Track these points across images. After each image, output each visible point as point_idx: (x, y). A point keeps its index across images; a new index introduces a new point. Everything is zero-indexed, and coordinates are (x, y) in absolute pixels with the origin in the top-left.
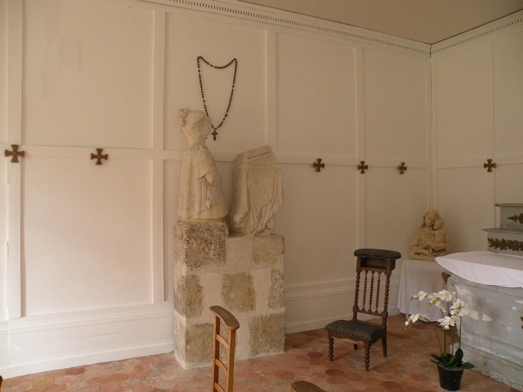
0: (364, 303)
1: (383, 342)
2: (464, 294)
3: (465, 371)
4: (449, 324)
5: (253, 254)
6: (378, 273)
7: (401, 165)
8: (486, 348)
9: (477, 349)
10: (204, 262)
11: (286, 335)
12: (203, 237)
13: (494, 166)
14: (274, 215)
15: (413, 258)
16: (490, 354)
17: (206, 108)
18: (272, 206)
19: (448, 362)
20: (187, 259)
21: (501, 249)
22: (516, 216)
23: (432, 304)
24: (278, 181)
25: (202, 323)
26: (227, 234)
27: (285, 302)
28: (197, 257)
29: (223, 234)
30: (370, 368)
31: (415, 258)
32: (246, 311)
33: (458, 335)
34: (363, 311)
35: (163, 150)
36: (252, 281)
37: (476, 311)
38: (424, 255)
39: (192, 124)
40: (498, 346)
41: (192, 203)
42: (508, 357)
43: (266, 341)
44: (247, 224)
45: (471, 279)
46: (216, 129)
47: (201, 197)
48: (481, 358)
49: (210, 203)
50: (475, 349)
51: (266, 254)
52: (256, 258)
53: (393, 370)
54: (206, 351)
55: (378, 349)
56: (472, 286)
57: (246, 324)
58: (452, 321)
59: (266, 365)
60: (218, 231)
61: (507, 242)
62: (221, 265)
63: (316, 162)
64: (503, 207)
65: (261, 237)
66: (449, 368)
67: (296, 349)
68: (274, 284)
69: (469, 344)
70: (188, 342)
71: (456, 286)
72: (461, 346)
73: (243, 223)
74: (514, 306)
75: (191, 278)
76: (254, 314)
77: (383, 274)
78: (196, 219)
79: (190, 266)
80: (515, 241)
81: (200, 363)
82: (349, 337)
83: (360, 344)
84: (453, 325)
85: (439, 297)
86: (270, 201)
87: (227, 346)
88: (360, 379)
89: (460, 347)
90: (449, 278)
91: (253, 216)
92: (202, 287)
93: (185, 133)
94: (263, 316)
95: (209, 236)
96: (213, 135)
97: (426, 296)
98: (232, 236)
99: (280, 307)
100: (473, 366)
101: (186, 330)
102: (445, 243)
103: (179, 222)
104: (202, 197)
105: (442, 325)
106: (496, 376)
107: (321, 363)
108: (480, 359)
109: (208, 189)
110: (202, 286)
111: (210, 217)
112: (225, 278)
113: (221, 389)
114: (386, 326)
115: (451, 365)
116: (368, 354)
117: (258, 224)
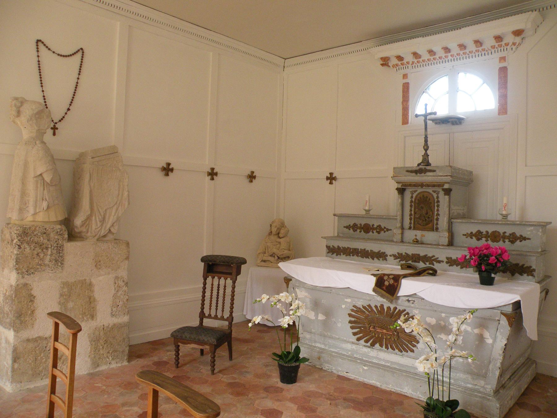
0: (210, 309)
3: (302, 365)
4: (287, 323)
5: (94, 260)
6: (224, 279)
7: (250, 174)
9: (313, 345)
10: (38, 269)
11: (130, 346)
12: (37, 241)
14: (118, 219)
17: (45, 99)
18: (117, 210)
19: (287, 358)
20: (17, 266)
21: (337, 255)
22: (350, 225)
23: (273, 306)
24: (124, 184)
25: (34, 337)
26: (66, 238)
27: (128, 311)
28: (30, 263)
29: (61, 239)
30: (215, 371)
31: (261, 265)
32: (86, 321)
33: (296, 329)
34: (210, 316)
36: (93, 289)
37: (313, 311)
38: (270, 262)
40: (330, 341)
43: (108, 353)
44: (89, 227)
46: (56, 123)
47: (36, 197)
48: (316, 354)
50: (311, 346)
51: (108, 259)
52: (98, 265)
53: (238, 371)
54: (38, 368)
55: (224, 354)
56: (310, 289)
57: (86, 335)
58: (290, 320)
59: (107, 378)
60: (55, 234)
61: (342, 248)
62: (58, 272)
63: (165, 166)
64: (341, 216)
65: (103, 242)
66: (288, 364)
67: (140, 359)
68: (117, 291)
69: (307, 342)
70: (15, 359)
71: (297, 289)
73: (85, 227)
75: (21, 287)
76: (95, 324)
77: (229, 279)
79: (21, 273)
80: (348, 248)
81: (30, 383)
82: (195, 343)
83: (206, 348)
84: (291, 323)
86: (115, 205)
87: (68, 353)
88: (206, 382)
90: (291, 282)
91: (96, 219)
92: (35, 297)
94: (105, 326)
95: (44, 240)
96: (53, 130)
97: (269, 299)
98: (71, 240)
99: (123, 316)
101: (13, 346)
103: (8, 224)
106: (327, 367)
107: (166, 370)
108: (316, 355)
109: (46, 188)
110: (35, 295)
111: (47, 220)
112: (62, 286)
113: (59, 400)
114: (231, 331)
115: (289, 361)
116: (213, 358)
117: (100, 228)
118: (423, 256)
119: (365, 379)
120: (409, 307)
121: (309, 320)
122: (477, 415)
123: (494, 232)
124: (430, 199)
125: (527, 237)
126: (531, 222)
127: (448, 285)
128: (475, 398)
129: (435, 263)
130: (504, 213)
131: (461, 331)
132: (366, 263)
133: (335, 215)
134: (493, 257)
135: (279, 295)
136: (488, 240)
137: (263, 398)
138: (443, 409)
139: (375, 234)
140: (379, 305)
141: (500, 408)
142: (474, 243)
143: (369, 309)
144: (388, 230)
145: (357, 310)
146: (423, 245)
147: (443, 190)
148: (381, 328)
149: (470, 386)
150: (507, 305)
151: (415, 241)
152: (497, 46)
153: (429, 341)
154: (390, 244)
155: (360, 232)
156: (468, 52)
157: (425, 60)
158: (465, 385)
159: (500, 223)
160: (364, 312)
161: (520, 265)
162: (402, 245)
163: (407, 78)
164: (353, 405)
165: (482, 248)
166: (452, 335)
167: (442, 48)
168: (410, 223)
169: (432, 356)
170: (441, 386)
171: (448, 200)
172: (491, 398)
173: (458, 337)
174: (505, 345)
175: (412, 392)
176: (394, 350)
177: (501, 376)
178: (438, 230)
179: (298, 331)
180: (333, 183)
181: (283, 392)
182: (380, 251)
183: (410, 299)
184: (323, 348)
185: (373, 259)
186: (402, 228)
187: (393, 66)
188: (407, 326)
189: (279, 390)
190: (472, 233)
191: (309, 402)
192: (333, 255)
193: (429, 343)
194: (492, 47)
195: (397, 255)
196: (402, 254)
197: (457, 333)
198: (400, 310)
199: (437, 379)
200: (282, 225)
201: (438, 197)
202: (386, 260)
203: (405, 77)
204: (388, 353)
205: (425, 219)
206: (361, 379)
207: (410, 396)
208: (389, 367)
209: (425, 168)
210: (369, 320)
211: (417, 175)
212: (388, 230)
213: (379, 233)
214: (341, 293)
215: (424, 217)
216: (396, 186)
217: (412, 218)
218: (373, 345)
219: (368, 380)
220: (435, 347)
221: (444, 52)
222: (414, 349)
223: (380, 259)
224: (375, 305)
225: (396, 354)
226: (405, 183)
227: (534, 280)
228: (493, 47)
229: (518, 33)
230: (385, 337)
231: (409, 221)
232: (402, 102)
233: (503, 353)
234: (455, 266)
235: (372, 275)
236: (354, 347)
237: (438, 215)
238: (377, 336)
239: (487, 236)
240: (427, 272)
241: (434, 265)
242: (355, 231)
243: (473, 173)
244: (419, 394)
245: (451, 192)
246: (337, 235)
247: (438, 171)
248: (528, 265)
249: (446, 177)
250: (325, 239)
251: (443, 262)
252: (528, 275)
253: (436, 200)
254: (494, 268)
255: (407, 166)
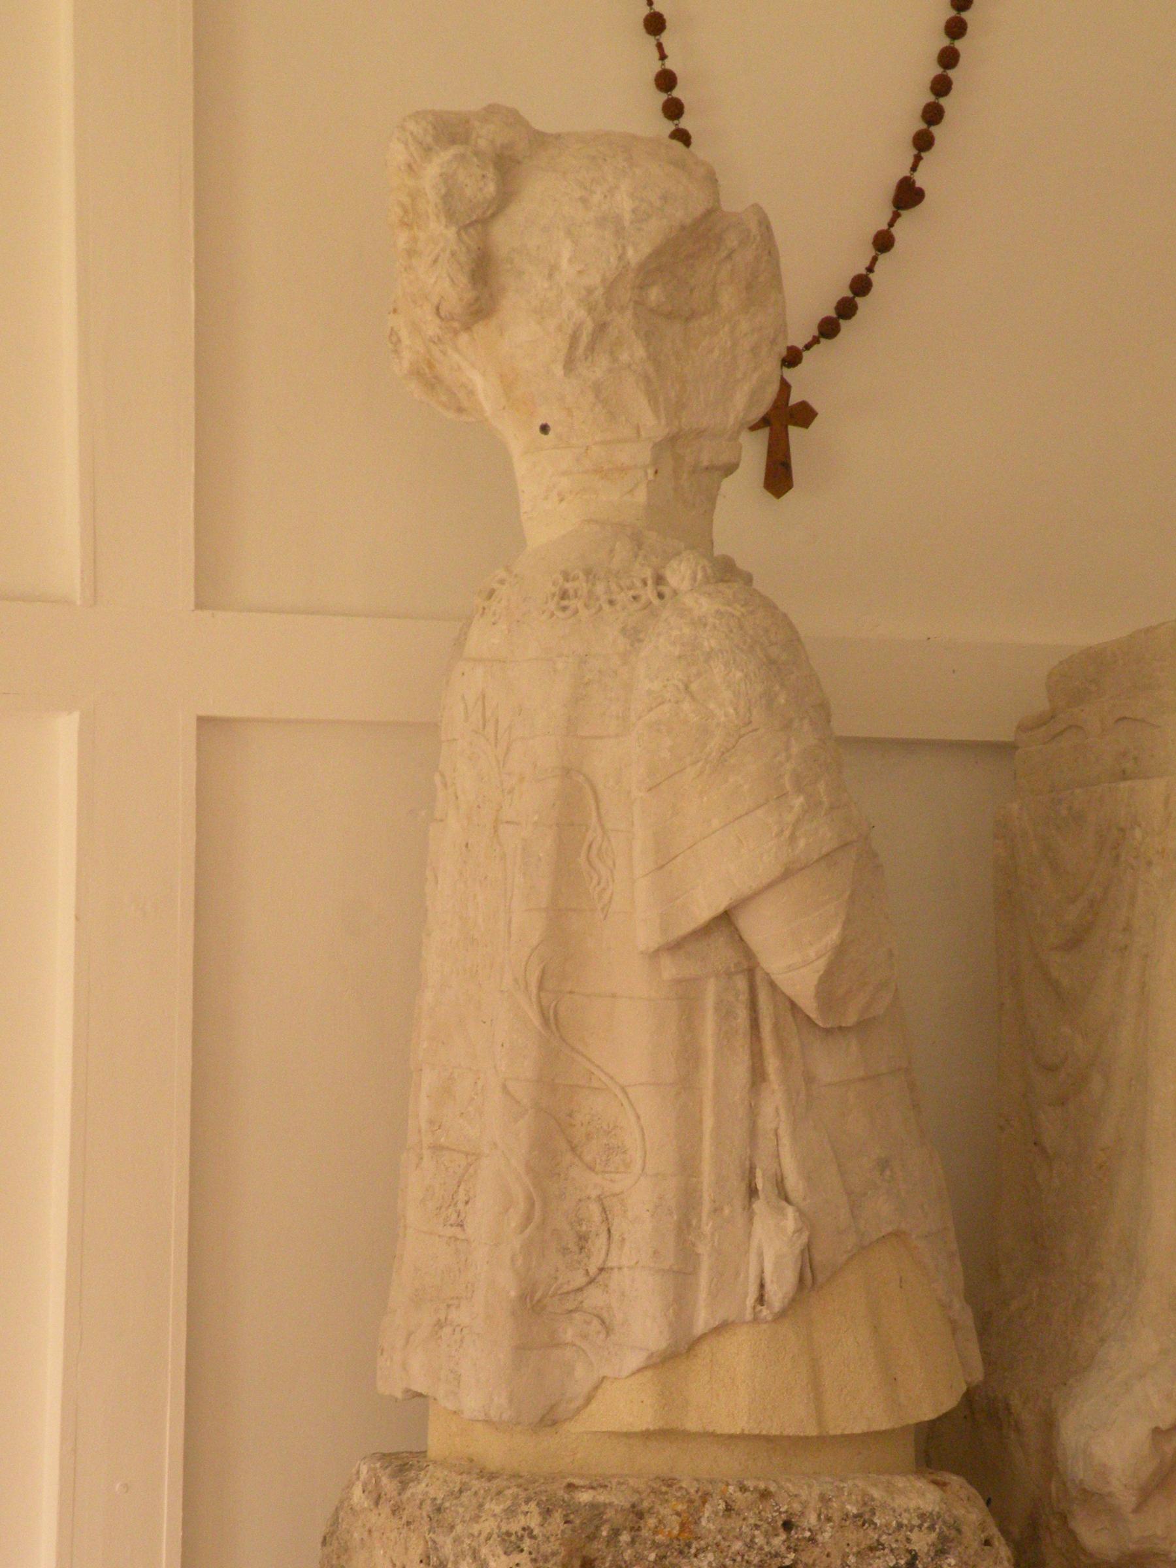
35: (199, 605)
39: (570, 302)
41: (583, 1239)
47: (688, 1166)
49: (804, 1238)
78: (629, 1435)
93: (487, 407)
104: (706, 1167)
109: (772, 1065)
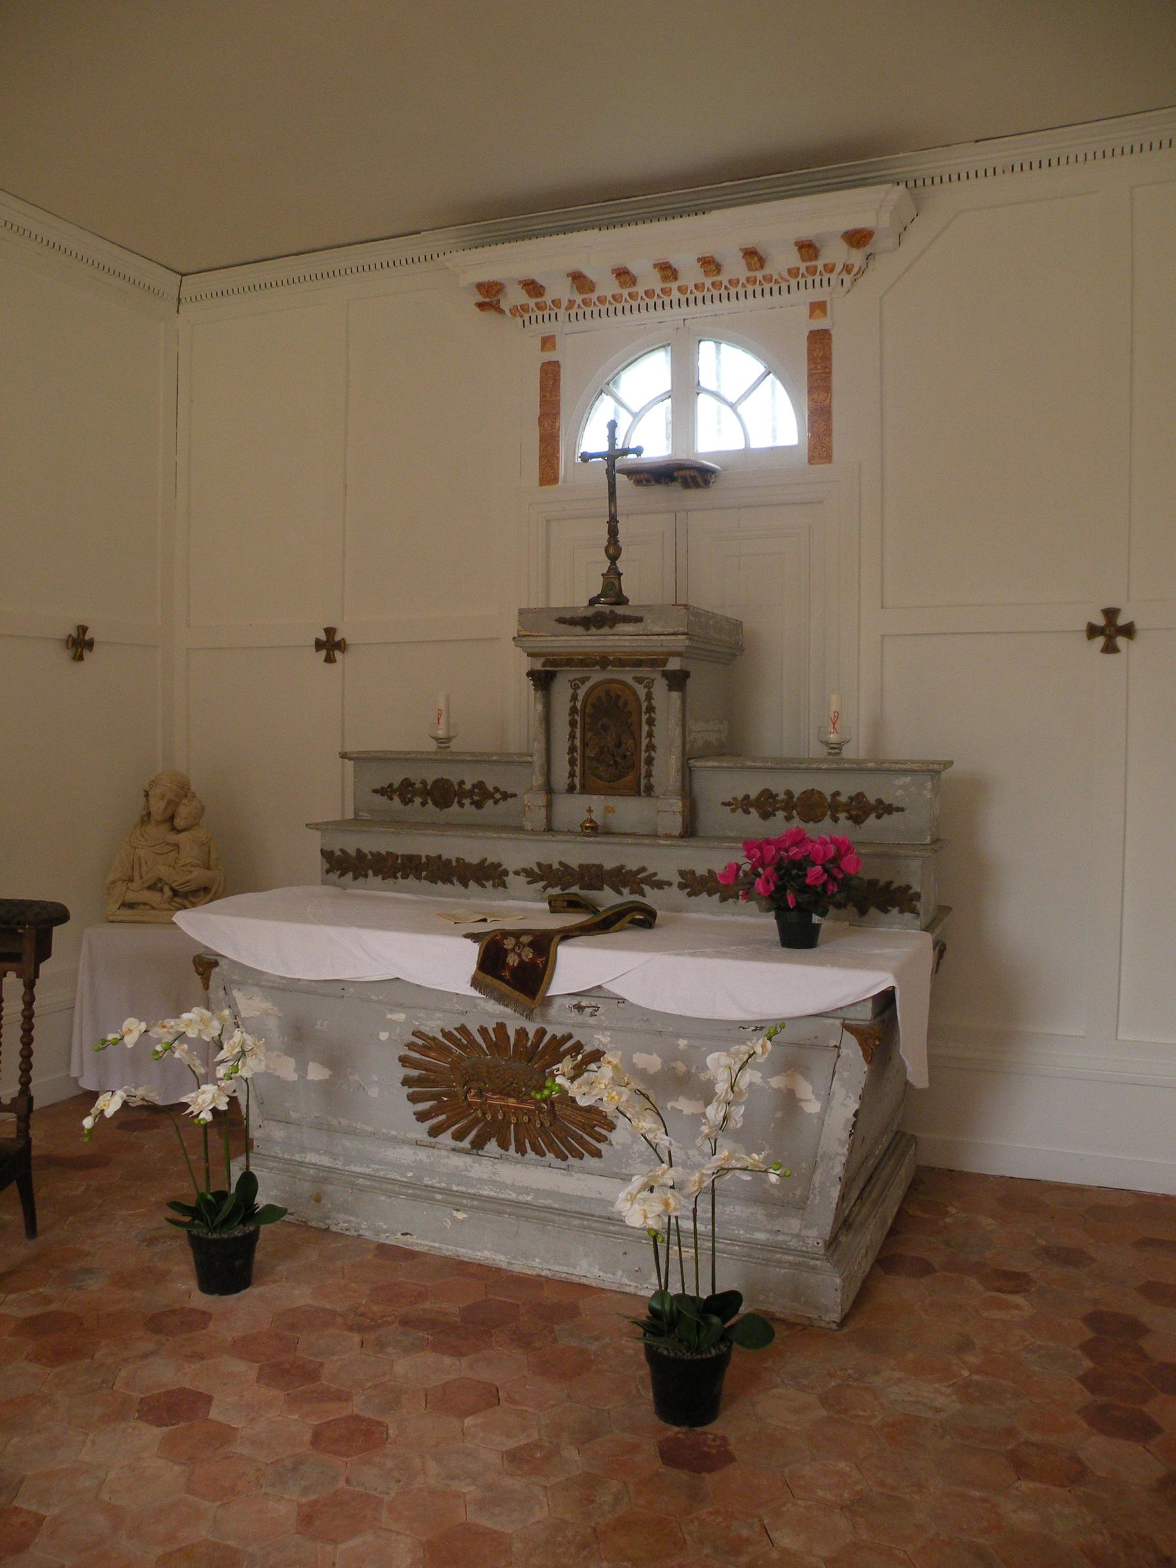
1: (21, 1191)
2: (258, 1014)
3: (265, 1229)
7: (75, 634)
8: (320, 1155)
9: (295, 1161)
13: (341, 646)
15: (115, 918)
16: (331, 1170)
19: (217, 1213)
21: (355, 878)
22: (391, 786)
23: (161, 1054)
31: (120, 918)
37: (290, 1056)
38: (147, 907)
40: (348, 1143)
42: (373, 1166)
45: (272, 966)
55: (7, 1217)
56: (278, 988)
58: (219, 1095)
61: (370, 857)
64: (361, 759)
69: (277, 1151)
71: (235, 993)
72: (252, 1161)
74: (384, 1030)
80: (389, 854)
84: (223, 1107)
85: (183, 1030)
89: (248, 1166)
90: (216, 970)
100: (284, 1212)
102: (208, 869)
105: (192, 1112)
114: (29, 1141)
118: (612, 869)
119: (463, 1247)
120: (583, 1025)
121: (284, 1085)
122: (782, 1316)
123: (809, 794)
124: (626, 703)
125: (896, 805)
126: (904, 762)
127: (693, 955)
128: (778, 1270)
129: (647, 888)
130: (833, 737)
131: (740, 1090)
132: (440, 896)
133: (344, 756)
134: (817, 867)
135: (179, 1018)
136: (794, 817)
137: (145, 1356)
138: (698, 1324)
139: (469, 807)
140: (491, 1026)
141: (843, 1287)
142: (754, 825)
143: (463, 1040)
144: (505, 796)
145: (426, 1044)
146: (611, 839)
147: (666, 675)
148: (500, 1093)
149: (761, 1236)
150: (859, 1002)
151: (587, 828)
152: (803, 270)
153: (650, 1130)
154: (515, 839)
155: (423, 804)
156: (726, 282)
157: (606, 297)
158: (749, 1236)
159: (825, 766)
160: (448, 1049)
161: (882, 883)
162: (552, 841)
163: (554, 346)
164: (431, 1338)
165: (784, 841)
166: (715, 1104)
167: (655, 266)
168: (572, 775)
169: (663, 1174)
170: (675, 1235)
171: (679, 702)
172: (819, 1263)
173: (733, 1108)
174: (856, 1115)
175: (601, 1274)
176: (543, 1155)
177: (843, 1197)
178: (652, 794)
179: (247, 1119)
180: (336, 657)
181: (212, 1326)
182: (485, 860)
183: (583, 1004)
184: (329, 1165)
185: (466, 885)
186: (549, 789)
187: (515, 311)
188: (585, 1089)
189: (198, 1320)
190: (747, 797)
191: (296, 1347)
192: (342, 878)
193: (650, 1136)
194: (789, 271)
195: (536, 870)
196: (550, 866)
197: (731, 1097)
198: (554, 1037)
199: (675, 1228)
200: (184, 791)
201: (649, 697)
202: (505, 887)
203: (548, 345)
204: (525, 1164)
205: (615, 762)
206: (448, 1250)
207: (594, 1284)
208: (531, 1205)
209: (612, 612)
210: (464, 1072)
211: (589, 632)
212: (505, 796)
213: (478, 805)
214: (374, 998)
215: (613, 755)
216: (526, 664)
217: (577, 760)
218: (478, 1145)
219: (470, 1252)
220: (667, 1144)
221: (660, 277)
222: (601, 1146)
223: (486, 884)
224: (481, 1027)
225: (550, 1167)
226: (554, 655)
227: (918, 923)
228: (794, 272)
229: (858, 238)
230: (513, 1120)
231: (568, 768)
232: (539, 419)
233: (850, 1136)
234: (705, 895)
235: (467, 936)
236: (422, 1155)
237: (651, 747)
238: (489, 1117)
239: (790, 805)
240: (628, 918)
241: (644, 895)
242: (406, 802)
243: (744, 625)
244: (622, 1277)
245: (688, 682)
246: (352, 816)
247: (649, 621)
248: (903, 884)
249: (673, 637)
250: (318, 829)
251: (670, 884)
252: (901, 911)
253: (644, 705)
254: (818, 901)
255: (555, 603)
